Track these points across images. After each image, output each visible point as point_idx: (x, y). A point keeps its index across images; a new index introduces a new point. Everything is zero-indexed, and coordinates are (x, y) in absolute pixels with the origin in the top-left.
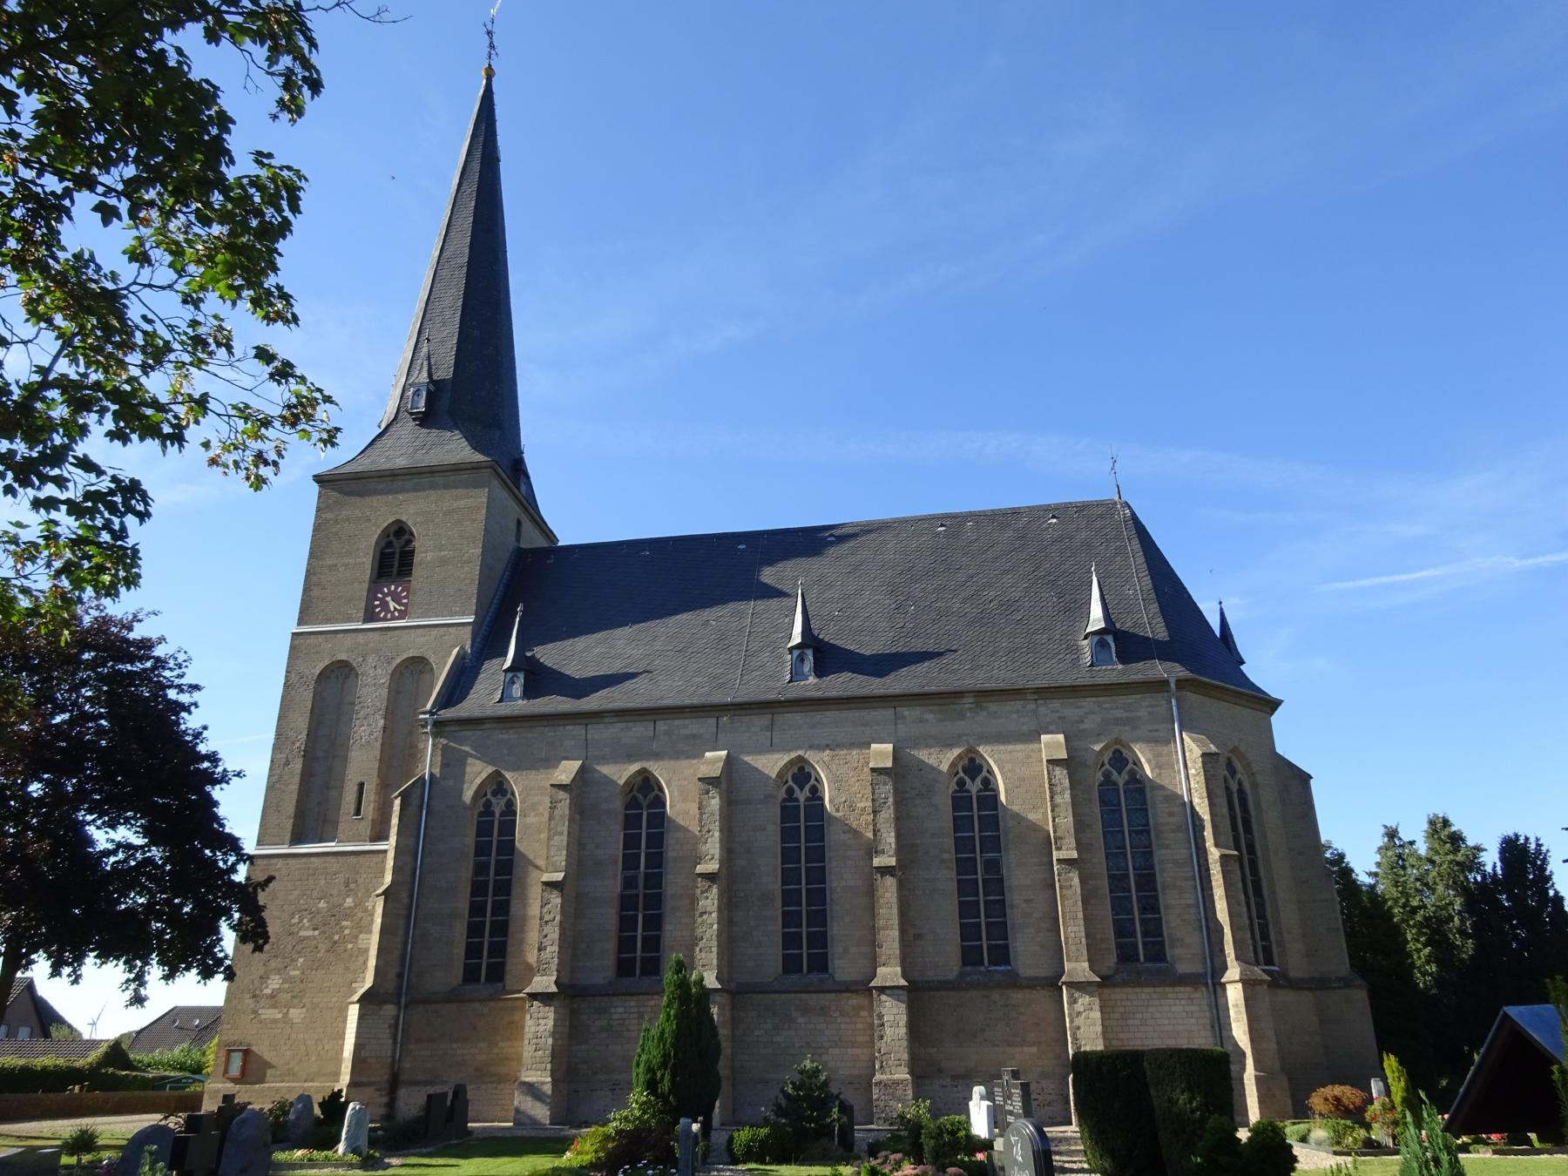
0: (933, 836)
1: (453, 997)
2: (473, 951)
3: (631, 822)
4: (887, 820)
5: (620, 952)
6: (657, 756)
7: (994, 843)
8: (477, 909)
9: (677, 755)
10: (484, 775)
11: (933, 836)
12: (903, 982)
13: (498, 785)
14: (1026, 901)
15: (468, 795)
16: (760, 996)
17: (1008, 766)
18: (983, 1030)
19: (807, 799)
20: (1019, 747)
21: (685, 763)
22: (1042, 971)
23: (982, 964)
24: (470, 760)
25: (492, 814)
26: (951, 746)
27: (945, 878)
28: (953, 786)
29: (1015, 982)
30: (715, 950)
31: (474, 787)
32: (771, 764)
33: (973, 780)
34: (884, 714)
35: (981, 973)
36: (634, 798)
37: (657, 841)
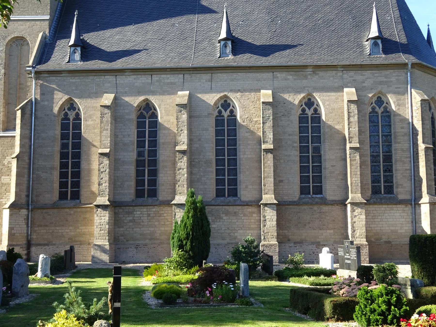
0: (289, 135)
1: (54, 206)
2: (63, 185)
3: (140, 125)
6: (153, 93)
7: (318, 139)
8: (64, 165)
9: (163, 93)
10: (64, 100)
11: (289, 135)
12: (276, 202)
13: (71, 105)
15: (56, 110)
17: (327, 103)
18: (309, 223)
19: (228, 116)
24: (56, 92)
25: (69, 120)
26: (300, 92)
28: (300, 112)
29: (324, 202)
31: (59, 106)
32: (211, 98)
35: (309, 198)
37: (154, 134)
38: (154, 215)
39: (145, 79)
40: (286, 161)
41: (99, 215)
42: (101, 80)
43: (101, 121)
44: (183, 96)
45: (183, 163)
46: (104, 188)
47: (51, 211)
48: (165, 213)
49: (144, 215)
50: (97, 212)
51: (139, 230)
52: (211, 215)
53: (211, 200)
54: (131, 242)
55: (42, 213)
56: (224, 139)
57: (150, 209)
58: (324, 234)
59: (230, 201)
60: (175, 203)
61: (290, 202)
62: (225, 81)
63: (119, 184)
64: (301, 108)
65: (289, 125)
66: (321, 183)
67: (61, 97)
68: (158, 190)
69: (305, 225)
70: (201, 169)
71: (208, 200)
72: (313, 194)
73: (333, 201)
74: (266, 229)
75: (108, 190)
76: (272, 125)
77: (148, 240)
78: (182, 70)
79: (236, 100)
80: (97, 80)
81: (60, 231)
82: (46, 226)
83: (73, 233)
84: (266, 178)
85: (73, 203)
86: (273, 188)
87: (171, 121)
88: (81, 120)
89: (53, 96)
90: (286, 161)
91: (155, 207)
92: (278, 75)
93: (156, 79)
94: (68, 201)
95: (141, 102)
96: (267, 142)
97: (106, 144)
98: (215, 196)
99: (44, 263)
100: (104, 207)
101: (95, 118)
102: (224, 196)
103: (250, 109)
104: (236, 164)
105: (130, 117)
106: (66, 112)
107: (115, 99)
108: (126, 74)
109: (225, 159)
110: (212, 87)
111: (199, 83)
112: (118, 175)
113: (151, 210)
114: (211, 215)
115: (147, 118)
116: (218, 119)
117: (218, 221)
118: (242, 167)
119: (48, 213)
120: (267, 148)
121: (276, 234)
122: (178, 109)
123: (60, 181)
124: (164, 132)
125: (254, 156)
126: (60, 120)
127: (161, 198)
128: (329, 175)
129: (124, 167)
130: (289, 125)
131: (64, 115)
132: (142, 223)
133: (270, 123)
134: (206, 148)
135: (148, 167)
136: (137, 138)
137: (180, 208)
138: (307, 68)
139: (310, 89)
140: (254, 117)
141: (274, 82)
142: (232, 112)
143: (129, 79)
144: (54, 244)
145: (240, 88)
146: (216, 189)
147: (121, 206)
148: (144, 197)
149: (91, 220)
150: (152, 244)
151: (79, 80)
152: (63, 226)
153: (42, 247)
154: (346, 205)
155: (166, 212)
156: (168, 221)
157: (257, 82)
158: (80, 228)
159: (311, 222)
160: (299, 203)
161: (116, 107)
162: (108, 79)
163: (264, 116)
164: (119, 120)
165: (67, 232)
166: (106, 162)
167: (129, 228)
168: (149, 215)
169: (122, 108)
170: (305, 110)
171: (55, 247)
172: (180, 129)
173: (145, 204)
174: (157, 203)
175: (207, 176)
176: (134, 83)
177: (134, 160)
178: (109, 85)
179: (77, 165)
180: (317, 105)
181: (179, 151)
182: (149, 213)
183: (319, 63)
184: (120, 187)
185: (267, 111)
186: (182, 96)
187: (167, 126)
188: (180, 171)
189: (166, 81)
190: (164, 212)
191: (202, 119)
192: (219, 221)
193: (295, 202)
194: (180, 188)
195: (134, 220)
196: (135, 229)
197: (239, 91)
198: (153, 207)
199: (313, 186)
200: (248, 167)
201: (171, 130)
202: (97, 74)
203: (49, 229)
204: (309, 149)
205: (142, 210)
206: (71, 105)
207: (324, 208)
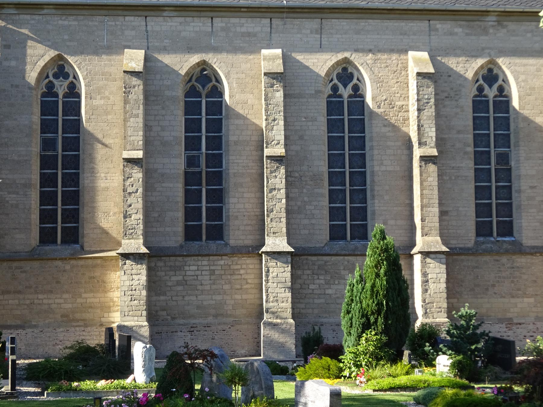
0: (459, 132)
1: (32, 256)
2: (47, 217)
3: (191, 108)
4: (429, 118)
5: (186, 220)
6: (216, 50)
7: (504, 140)
8: (47, 180)
9: (235, 50)
10: (47, 58)
11: (459, 132)
12: (444, 249)
13: (60, 69)
14: (532, 187)
15: (32, 75)
16: (314, 258)
17: (522, 77)
18: (493, 286)
19: (350, 96)
20: (531, 61)
21: (241, 57)
22: (249, 240)
23: (491, 235)
24: (30, 43)
25: (57, 96)
26: (476, 57)
27: (468, 166)
28: (474, 92)
29: (519, 249)
30: (284, 220)
31: (38, 68)
32: (321, 63)
33: (345, 86)
34: (422, 25)
35: (492, 242)
36: (193, 87)
37: (216, 126)
38: (223, 272)
39: (201, 24)
40: (453, 178)
41: (128, 272)
42: (117, 23)
43: (125, 100)
44: (273, 58)
45: (277, 180)
46: (134, 222)
47: (27, 265)
48: (241, 269)
49: (204, 273)
50: (125, 267)
51: (194, 298)
52: (323, 272)
53: (322, 245)
54: (182, 321)
55: (10, 268)
56: (344, 137)
57: (214, 261)
58: (519, 305)
59: (356, 248)
60: (269, 250)
61: (460, 249)
62: (345, 33)
63: (156, 215)
64: (331, 84)
65: (457, 114)
66: (511, 216)
67: (42, 52)
68: (225, 228)
69: (487, 289)
70: (305, 191)
71: (317, 246)
72: (498, 235)
73: (534, 247)
74: (428, 296)
75: (141, 226)
76: (434, 114)
77: (211, 318)
78: (269, 10)
79: (366, 67)
80: (110, 23)
81: (45, 301)
82: (19, 292)
83: (70, 306)
84: (426, 206)
85: (67, 250)
86: (437, 225)
87: (249, 102)
88: (79, 96)
89: (26, 51)
90: (453, 178)
91: (224, 257)
92: (439, 26)
93: (220, 25)
94: (59, 247)
95: (193, 68)
96: (426, 145)
97: (136, 142)
98: (328, 238)
99: (147, 357)
100: (136, 257)
101: (107, 93)
102: (344, 238)
103: (389, 84)
104: (365, 181)
105: (174, 94)
106: (50, 82)
107: (147, 59)
108: (165, 14)
109: (344, 172)
110: (323, 43)
111: (299, 35)
112: (153, 199)
113: (215, 263)
114: (323, 272)
115: (204, 96)
116: (331, 102)
117: (336, 282)
118: (376, 188)
119: (21, 268)
120: (427, 154)
121: (445, 305)
122: (267, 81)
123: (40, 210)
124: (237, 122)
125: (398, 168)
126: (39, 97)
127: (232, 242)
128: (526, 203)
129: (164, 185)
130: (457, 114)
131: (69, 88)
132: (199, 287)
133: (430, 110)
134: (314, 153)
135: (207, 185)
136: (185, 132)
137: (276, 259)
138: (488, 15)
139: (492, 53)
140: (397, 99)
141: (432, 37)
142: (356, 88)
143: (170, 24)
144: (35, 326)
145: (372, 47)
146: (330, 225)
147: (161, 257)
148: (201, 239)
149: (104, 282)
150: (219, 324)
151: (76, 23)
152: (51, 292)
153: (12, 331)
154: (411, 257)
155: (244, 266)
156: (247, 283)
157: (402, 37)
158: (84, 295)
159: (497, 285)
160: (477, 251)
161: (149, 73)
162: (131, 21)
163: (420, 97)
164: (153, 98)
165: (58, 304)
166: (137, 174)
167: (177, 296)
168: (212, 273)
169: (158, 77)
170: (338, 88)
171: (36, 331)
172: (271, 118)
173: (206, 253)
174: (228, 250)
175: (315, 203)
176: (180, 32)
177: (182, 172)
178: (133, 33)
179: (73, 180)
180: (503, 81)
181: (271, 158)
182: (212, 268)
183: (509, 8)
184: (158, 221)
185: (425, 89)
186: (271, 58)
187: (241, 112)
188: (274, 193)
189: (238, 29)
190: (239, 267)
191: (305, 100)
192: (339, 283)
193: (469, 249)
194: (274, 224)
195: (186, 281)
196: (187, 298)
197: (370, 51)
198: (220, 258)
199: (498, 222)
200: (387, 187)
201: (249, 119)
202: (111, 12)
203: (24, 299)
204: (489, 158)
205: (200, 263)
206: (60, 69)
207: (519, 260)
